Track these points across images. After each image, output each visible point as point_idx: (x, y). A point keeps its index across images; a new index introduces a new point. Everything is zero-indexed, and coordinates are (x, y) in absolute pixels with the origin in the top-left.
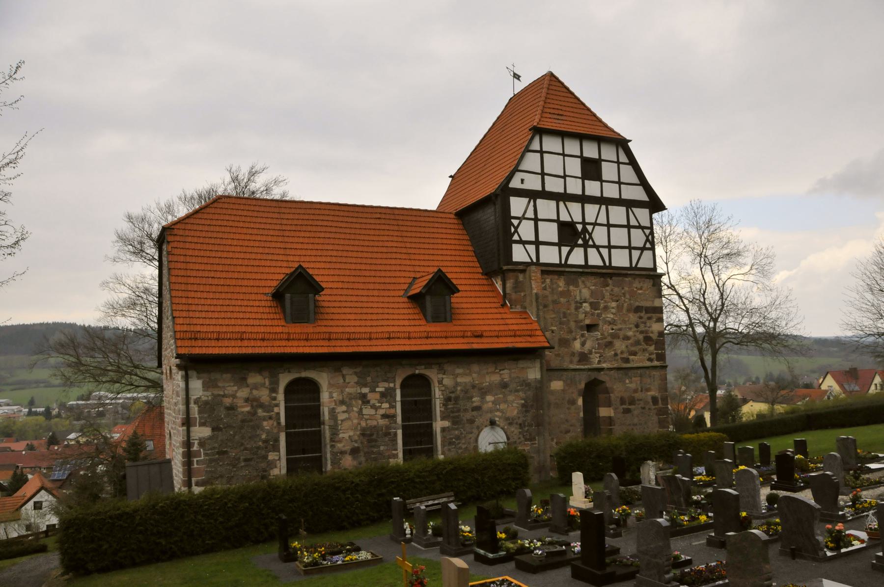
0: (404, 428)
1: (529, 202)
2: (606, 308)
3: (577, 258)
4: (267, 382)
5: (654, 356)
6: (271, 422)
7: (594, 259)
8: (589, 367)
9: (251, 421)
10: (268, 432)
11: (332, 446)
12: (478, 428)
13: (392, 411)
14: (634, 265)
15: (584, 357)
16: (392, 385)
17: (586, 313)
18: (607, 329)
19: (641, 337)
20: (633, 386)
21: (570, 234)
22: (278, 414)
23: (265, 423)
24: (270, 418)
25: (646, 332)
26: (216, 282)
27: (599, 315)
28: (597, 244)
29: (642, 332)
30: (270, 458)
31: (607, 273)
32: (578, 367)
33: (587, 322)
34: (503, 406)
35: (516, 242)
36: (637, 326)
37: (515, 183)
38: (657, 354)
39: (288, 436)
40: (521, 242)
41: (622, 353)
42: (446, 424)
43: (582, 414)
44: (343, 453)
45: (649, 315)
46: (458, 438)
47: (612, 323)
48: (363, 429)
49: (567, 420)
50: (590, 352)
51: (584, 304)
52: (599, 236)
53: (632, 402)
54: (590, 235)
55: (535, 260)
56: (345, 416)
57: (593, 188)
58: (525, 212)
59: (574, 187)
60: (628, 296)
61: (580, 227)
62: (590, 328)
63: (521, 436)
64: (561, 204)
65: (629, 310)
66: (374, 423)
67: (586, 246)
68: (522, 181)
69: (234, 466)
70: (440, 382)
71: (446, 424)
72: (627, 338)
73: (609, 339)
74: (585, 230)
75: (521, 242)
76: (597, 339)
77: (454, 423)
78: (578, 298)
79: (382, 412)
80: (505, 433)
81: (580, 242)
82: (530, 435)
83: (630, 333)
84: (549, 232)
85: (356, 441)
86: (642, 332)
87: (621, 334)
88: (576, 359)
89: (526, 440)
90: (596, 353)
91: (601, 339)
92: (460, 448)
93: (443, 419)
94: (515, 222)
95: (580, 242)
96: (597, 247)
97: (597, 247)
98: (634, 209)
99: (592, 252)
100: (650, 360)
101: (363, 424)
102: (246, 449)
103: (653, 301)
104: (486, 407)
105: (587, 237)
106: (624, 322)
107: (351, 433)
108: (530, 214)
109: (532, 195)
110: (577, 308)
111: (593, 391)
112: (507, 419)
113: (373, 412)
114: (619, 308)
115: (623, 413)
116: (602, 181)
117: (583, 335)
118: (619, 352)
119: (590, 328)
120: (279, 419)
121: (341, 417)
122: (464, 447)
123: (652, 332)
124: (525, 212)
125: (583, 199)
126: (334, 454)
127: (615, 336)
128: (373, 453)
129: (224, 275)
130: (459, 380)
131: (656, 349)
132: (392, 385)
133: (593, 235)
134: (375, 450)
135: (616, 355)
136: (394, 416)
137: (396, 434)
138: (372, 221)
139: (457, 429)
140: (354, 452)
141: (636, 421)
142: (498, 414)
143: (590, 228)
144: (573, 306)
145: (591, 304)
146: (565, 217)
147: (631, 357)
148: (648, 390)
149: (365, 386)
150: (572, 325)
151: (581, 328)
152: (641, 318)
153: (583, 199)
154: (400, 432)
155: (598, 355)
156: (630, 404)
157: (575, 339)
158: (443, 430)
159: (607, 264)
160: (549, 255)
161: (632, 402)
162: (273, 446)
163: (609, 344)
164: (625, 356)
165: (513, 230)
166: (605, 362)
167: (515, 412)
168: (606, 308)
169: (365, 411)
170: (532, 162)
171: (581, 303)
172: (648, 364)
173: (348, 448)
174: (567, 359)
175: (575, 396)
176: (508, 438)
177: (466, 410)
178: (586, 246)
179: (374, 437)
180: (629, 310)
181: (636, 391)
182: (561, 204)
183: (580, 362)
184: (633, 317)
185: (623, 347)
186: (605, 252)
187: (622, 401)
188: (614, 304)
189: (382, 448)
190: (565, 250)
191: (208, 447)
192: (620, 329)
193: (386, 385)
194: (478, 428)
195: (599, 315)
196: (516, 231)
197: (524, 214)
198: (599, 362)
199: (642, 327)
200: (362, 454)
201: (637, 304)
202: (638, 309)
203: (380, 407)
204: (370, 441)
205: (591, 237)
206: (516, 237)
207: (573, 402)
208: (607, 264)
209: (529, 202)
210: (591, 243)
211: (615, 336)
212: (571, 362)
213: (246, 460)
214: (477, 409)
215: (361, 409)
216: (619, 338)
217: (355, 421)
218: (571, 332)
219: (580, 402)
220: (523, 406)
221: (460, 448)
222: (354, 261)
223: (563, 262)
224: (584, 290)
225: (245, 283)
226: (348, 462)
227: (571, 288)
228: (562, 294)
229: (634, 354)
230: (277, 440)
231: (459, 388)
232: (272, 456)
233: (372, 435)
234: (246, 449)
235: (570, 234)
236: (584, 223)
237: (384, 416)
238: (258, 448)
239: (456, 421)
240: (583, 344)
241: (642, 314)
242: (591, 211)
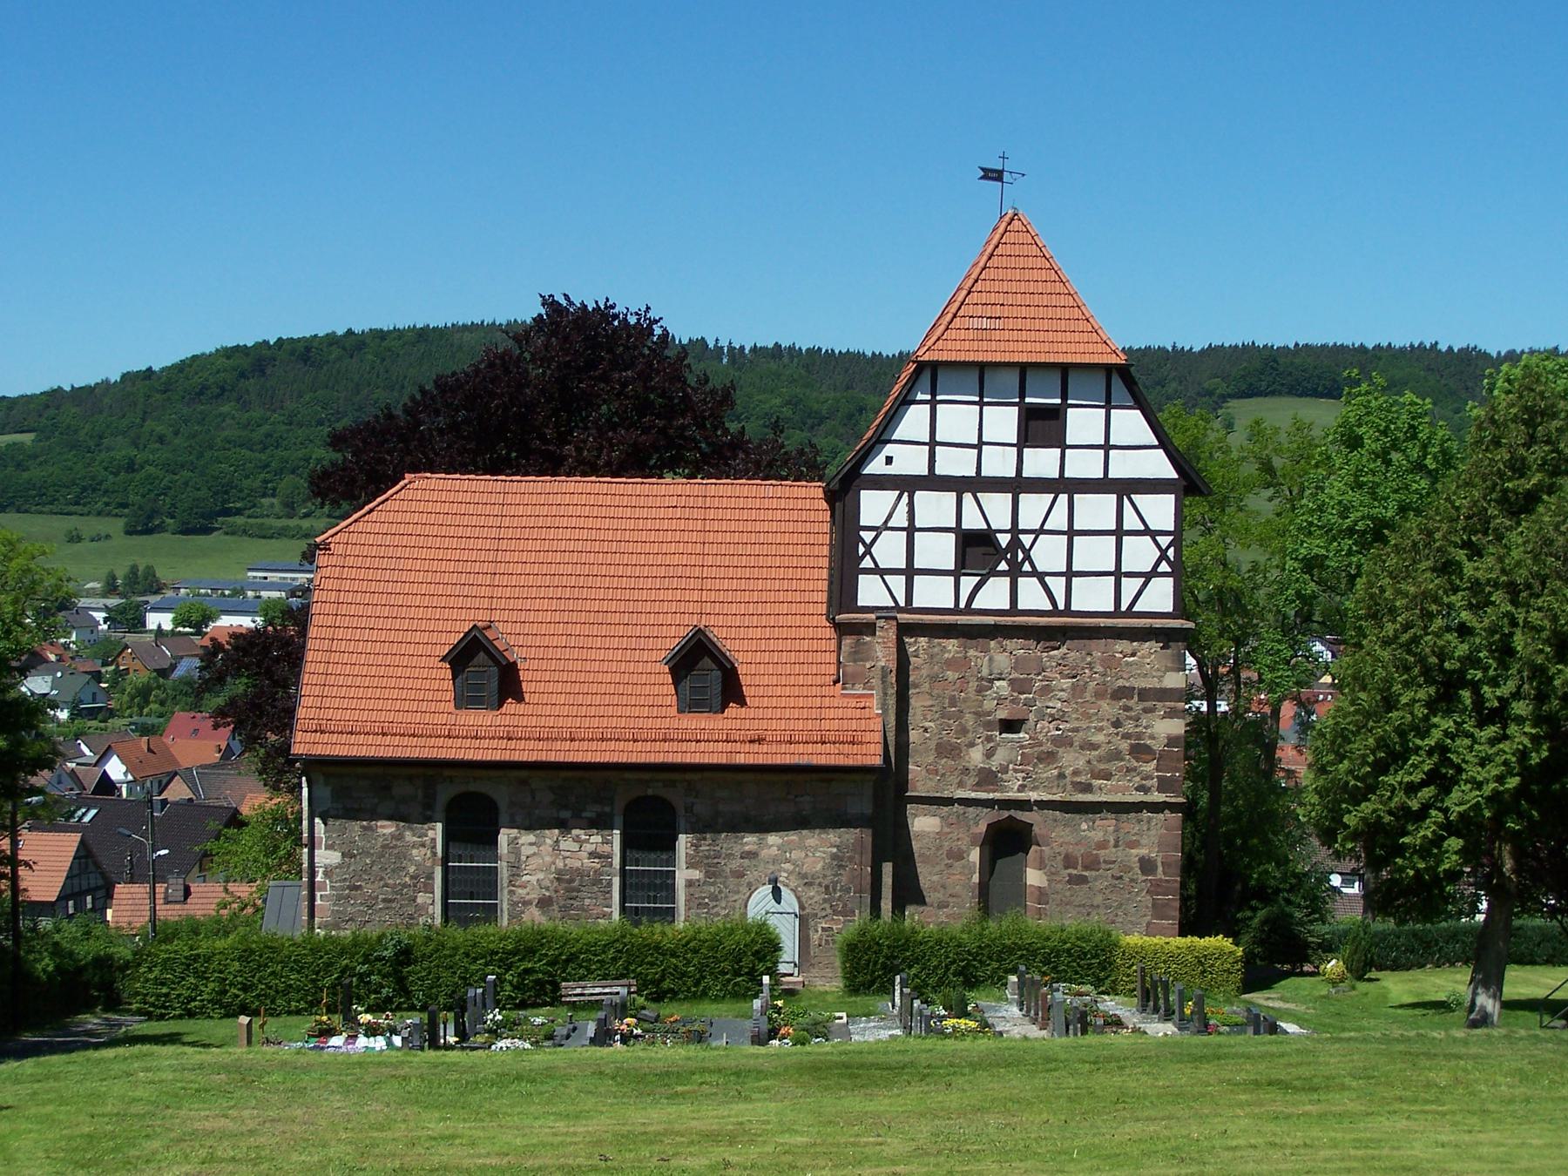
0: (623, 873)
1: (900, 497)
2: (1046, 690)
3: (995, 595)
4: (420, 793)
6: (423, 850)
7: (1031, 596)
8: (997, 795)
9: (395, 847)
10: (418, 865)
11: (511, 893)
12: (749, 885)
13: (607, 848)
14: (1124, 608)
15: (988, 778)
16: (607, 809)
17: (1000, 700)
18: (1047, 729)
19: (1124, 746)
20: (1097, 835)
21: (977, 551)
22: (434, 840)
23: (415, 852)
24: (423, 845)
25: (1139, 736)
26: (375, 635)
27: (1029, 704)
28: (1040, 569)
29: (1126, 736)
30: (419, 900)
31: (1060, 630)
32: (973, 795)
33: (1002, 714)
34: (796, 855)
35: (867, 571)
36: (1117, 724)
37: (876, 467)
39: (446, 871)
40: (877, 571)
41: (1076, 773)
42: (696, 874)
43: (976, 878)
44: (526, 903)
45: (1149, 704)
46: (714, 898)
47: (1060, 717)
48: (559, 872)
49: (944, 887)
50: (1005, 770)
51: (997, 683)
52: (1048, 553)
53: (1092, 864)
54: (1027, 552)
55: (902, 603)
56: (534, 849)
57: (1041, 463)
58: (890, 516)
59: (999, 464)
60: (1099, 669)
61: (1004, 540)
62: (1010, 726)
63: (827, 906)
64: (968, 498)
65: (1099, 695)
66: (578, 864)
67: (1015, 573)
68: (889, 460)
69: (370, 907)
70: (689, 809)
71: (696, 874)
73: (1048, 747)
74: (1015, 543)
75: (877, 571)
76: (1022, 747)
77: (708, 875)
78: (985, 672)
79: (589, 848)
80: (798, 898)
81: (1003, 566)
82: (845, 905)
83: (1099, 738)
84: (938, 551)
85: (547, 889)
86: (1126, 736)
87: (1078, 738)
88: (972, 781)
89: (835, 912)
90: (1016, 771)
91: (1031, 746)
92: (718, 914)
93: (690, 866)
94: (868, 536)
95: (1003, 566)
96: (1041, 576)
97: (1041, 576)
98: (1136, 498)
99: (1028, 586)
100: (1144, 789)
101: (560, 864)
102: (386, 885)
103: (1160, 678)
104: (764, 853)
105: (1021, 555)
106: (1088, 716)
107: (541, 876)
108: (900, 519)
109: (907, 485)
110: (980, 690)
111: (1008, 840)
112: (803, 876)
113: (575, 846)
114: (1077, 691)
115: (1069, 882)
116: (1064, 447)
117: (989, 739)
118: (1068, 772)
119: (1010, 726)
120: (434, 847)
121: (526, 851)
122: (723, 912)
123: (1152, 737)
124: (890, 516)
125: (1017, 485)
126: (514, 904)
127: (1063, 742)
128: (571, 907)
129: (389, 624)
130: (721, 807)
132: (607, 809)
134: (576, 904)
135: (1061, 776)
136: (610, 856)
137: (610, 884)
138: (662, 513)
139: (713, 884)
140: (544, 903)
141: (1098, 899)
142: (787, 866)
143: (1026, 540)
144: (973, 685)
145: (1012, 682)
146: (972, 521)
147: (1097, 783)
148: (1134, 845)
149: (566, 807)
150: (969, 720)
151: (988, 726)
152: (1127, 709)
153: (1017, 485)
154: (616, 881)
155: (1020, 775)
156: (1086, 868)
157: (972, 745)
158: (690, 884)
159: (1061, 606)
160: (934, 594)
161: (1092, 864)
162: (425, 885)
163: (1050, 757)
164: (1082, 779)
165: (861, 549)
166: (1034, 789)
167: (819, 867)
168: (1046, 690)
169: (563, 845)
170: (914, 421)
171: (991, 681)
172: (1139, 797)
173: (534, 896)
174: (954, 779)
175: (963, 844)
176: (802, 907)
177: (729, 856)
178: (1015, 573)
179: (576, 884)
180: (1099, 695)
181: (1102, 845)
182: (968, 498)
183: (978, 786)
184: (1109, 708)
185: (1081, 763)
186: (1056, 586)
187: (1069, 862)
188: (1066, 683)
189: (587, 901)
190: (968, 583)
191: (335, 878)
192: (1076, 730)
193: (598, 808)
194: (749, 885)
195: (1029, 704)
196: (868, 552)
197: (886, 522)
198: (1022, 788)
199: (1129, 727)
200: (555, 907)
201: (1121, 683)
202: (1121, 693)
203: (587, 841)
204: (568, 890)
205: (1028, 557)
206: (867, 563)
207: (959, 855)
208: (1061, 606)
209: (900, 497)
210: (1027, 567)
211: (1063, 742)
212: (961, 785)
213: (384, 900)
214: (752, 855)
215: (557, 841)
216: (1071, 745)
217: (548, 859)
218: (963, 731)
219: (975, 855)
220: (834, 857)
221: (718, 914)
222: (733, 526)
223: (962, 605)
224: (1001, 656)
225: (417, 637)
226: (534, 917)
227: (972, 652)
228: (950, 664)
229: (1107, 776)
230: (430, 877)
231: (720, 820)
232: (422, 898)
233: (571, 881)
234: (386, 885)
235: (977, 551)
236: (1015, 530)
237: (592, 855)
238: (405, 885)
239: (712, 873)
240: (989, 754)
241: (1131, 703)
242: (1033, 507)
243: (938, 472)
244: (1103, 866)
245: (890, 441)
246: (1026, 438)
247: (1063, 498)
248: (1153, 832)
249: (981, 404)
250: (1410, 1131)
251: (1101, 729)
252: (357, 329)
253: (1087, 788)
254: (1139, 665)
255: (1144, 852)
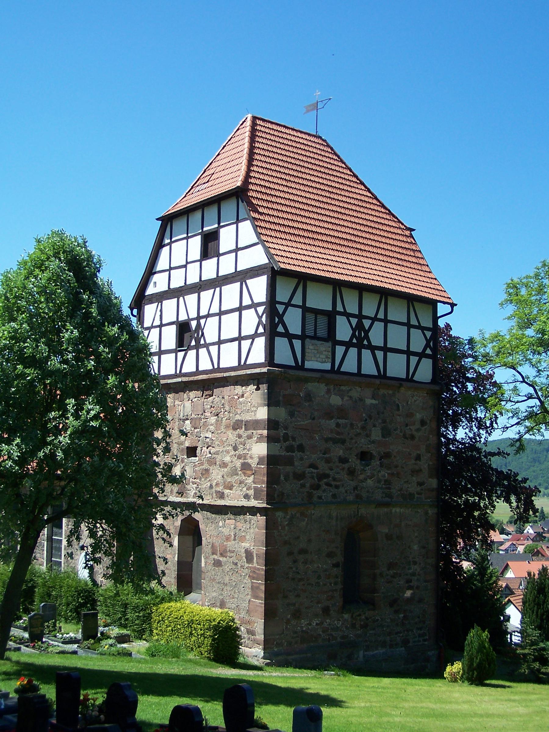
5: (251, 492)
36: (235, 449)
38: (256, 489)
45: (250, 432)
72: (224, 465)
83: (227, 459)
86: (239, 457)
94: (261, 330)
100: (247, 497)
105: (277, 320)
131: (254, 482)
133: (285, 318)
135: (211, 487)
152: (240, 436)
164: (220, 489)
184: (231, 435)
199: (240, 451)
201: (238, 417)
202: (237, 426)
206: (261, 309)
243: (307, 305)
244: (229, 554)
245: (155, 273)
246: (205, 254)
247: (218, 289)
248: (252, 530)
249: (187, 238)
250: (383, 692)
251: (228, 452)
252: (103, 276)
253: (221, 496)
254: (245, 403)
255: (246, 545)
